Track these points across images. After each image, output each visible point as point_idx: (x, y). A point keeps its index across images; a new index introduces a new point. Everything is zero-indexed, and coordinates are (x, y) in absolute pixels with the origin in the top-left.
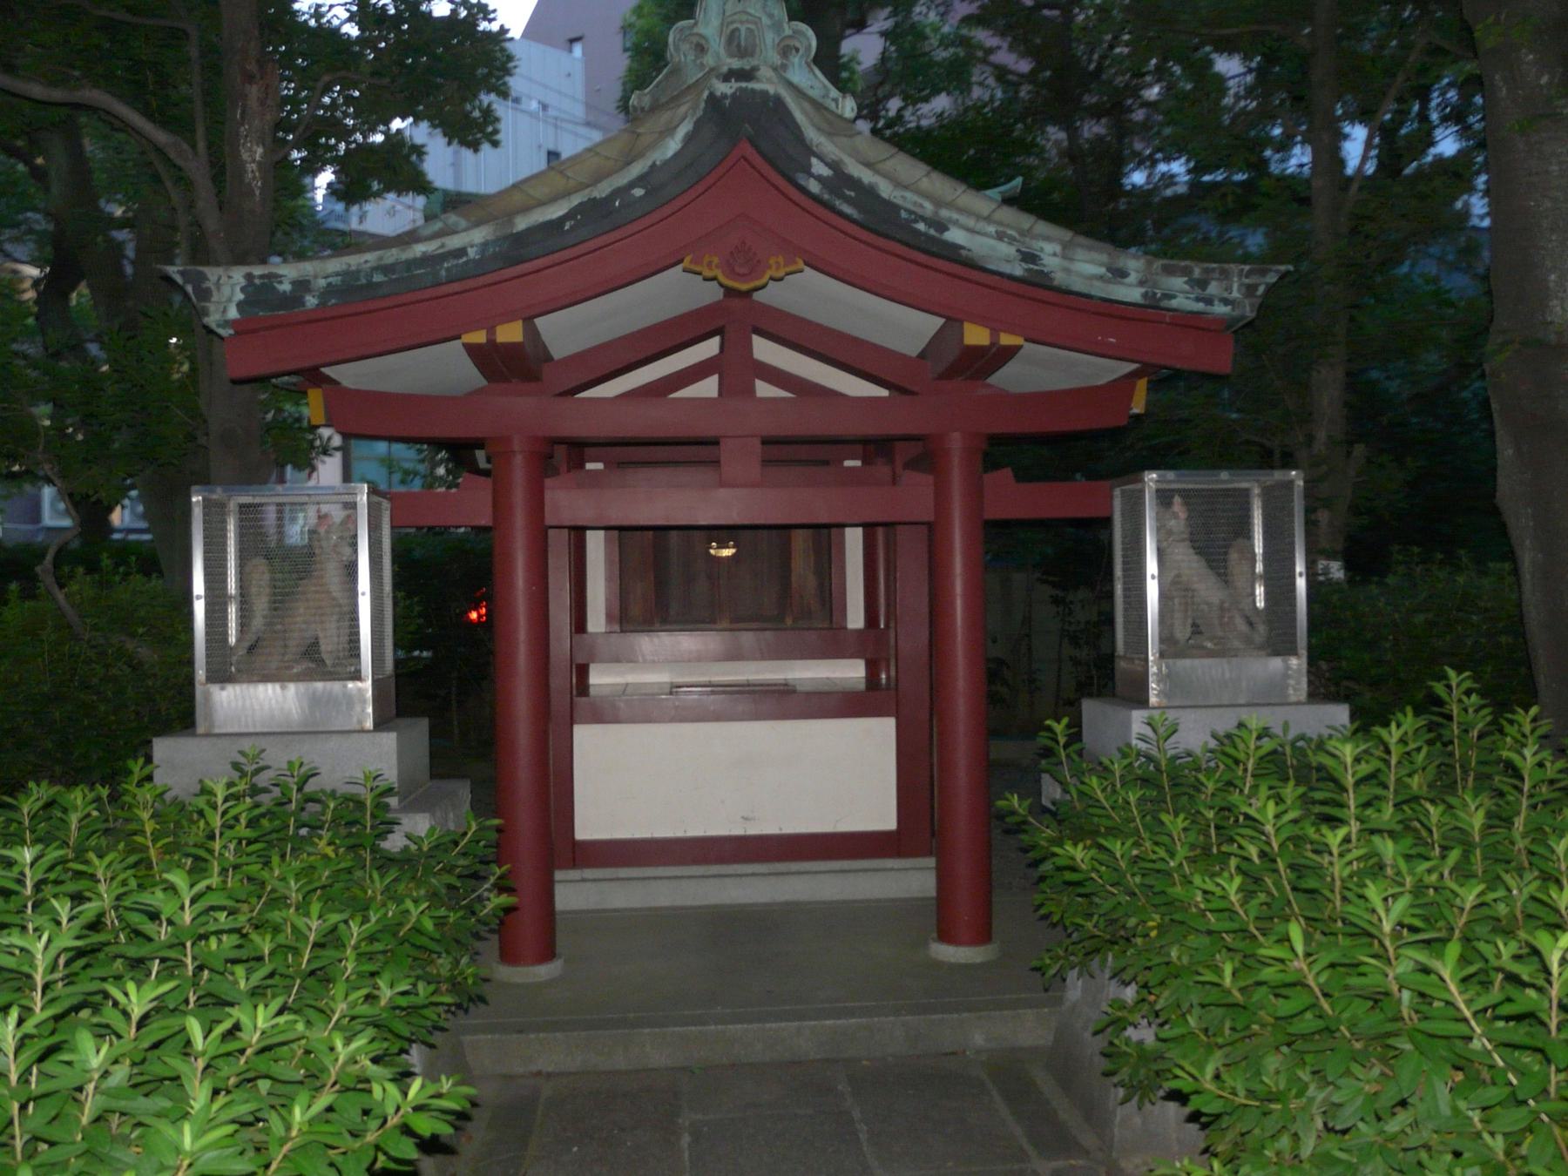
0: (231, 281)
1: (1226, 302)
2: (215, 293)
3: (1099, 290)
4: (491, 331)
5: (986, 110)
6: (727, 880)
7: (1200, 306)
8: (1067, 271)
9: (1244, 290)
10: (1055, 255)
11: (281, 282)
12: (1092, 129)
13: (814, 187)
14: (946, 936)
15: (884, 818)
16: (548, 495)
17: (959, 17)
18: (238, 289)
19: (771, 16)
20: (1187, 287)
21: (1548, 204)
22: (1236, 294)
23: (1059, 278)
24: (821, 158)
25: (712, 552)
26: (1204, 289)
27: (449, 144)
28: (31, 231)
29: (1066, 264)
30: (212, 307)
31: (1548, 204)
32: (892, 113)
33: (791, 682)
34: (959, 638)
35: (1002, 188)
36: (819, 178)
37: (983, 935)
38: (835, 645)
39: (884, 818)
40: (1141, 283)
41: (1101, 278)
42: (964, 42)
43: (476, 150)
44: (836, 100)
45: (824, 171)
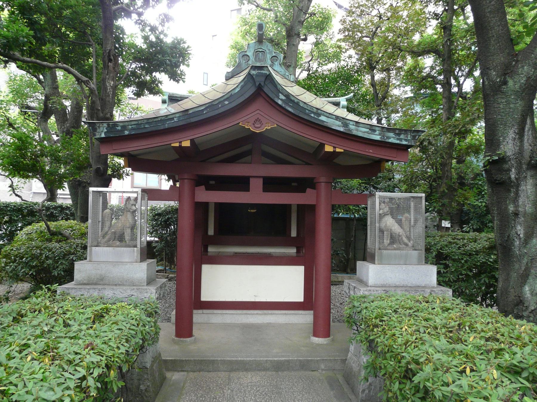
0: (103, 126)
1: (406, 140)
2: (98, 129)
3: (366, 136)
4: (180, 142)
5: (345, 69)
6: (248, 315)
7: (398, 142)
8: (357, 130)
9: (412, 137)
10: (353, 125)
11: (118, 127)
12: (378, 76)
13: (280, 102)
14: (315, 335)
15: (299, 297)
16: (196, 192)
17: (337, 39)
18: (105, 128)
19: (269, 50)
20: (394, 136)
21: (500, 117)
22: (409, 138)
23: (355, 133)
24: (283, 94)
25: (249, 210)
26: (400, 136)
27: (170, 80)
28: (37, 99)
29: (357, 127)
30: (97, 134)
31: (500, 117)
32: (314, 69)
33: (272, 253)
34: (254, 251)
35: (346, 97)
36: (281, 100)
37: (327, 334)
38: (288, 242)
39: (299, 297)
40: (380, 134)
41: (367, 133)
42: (339, 47)
43: (178, 82)
44: (288, 76)
45: (283, 98)
